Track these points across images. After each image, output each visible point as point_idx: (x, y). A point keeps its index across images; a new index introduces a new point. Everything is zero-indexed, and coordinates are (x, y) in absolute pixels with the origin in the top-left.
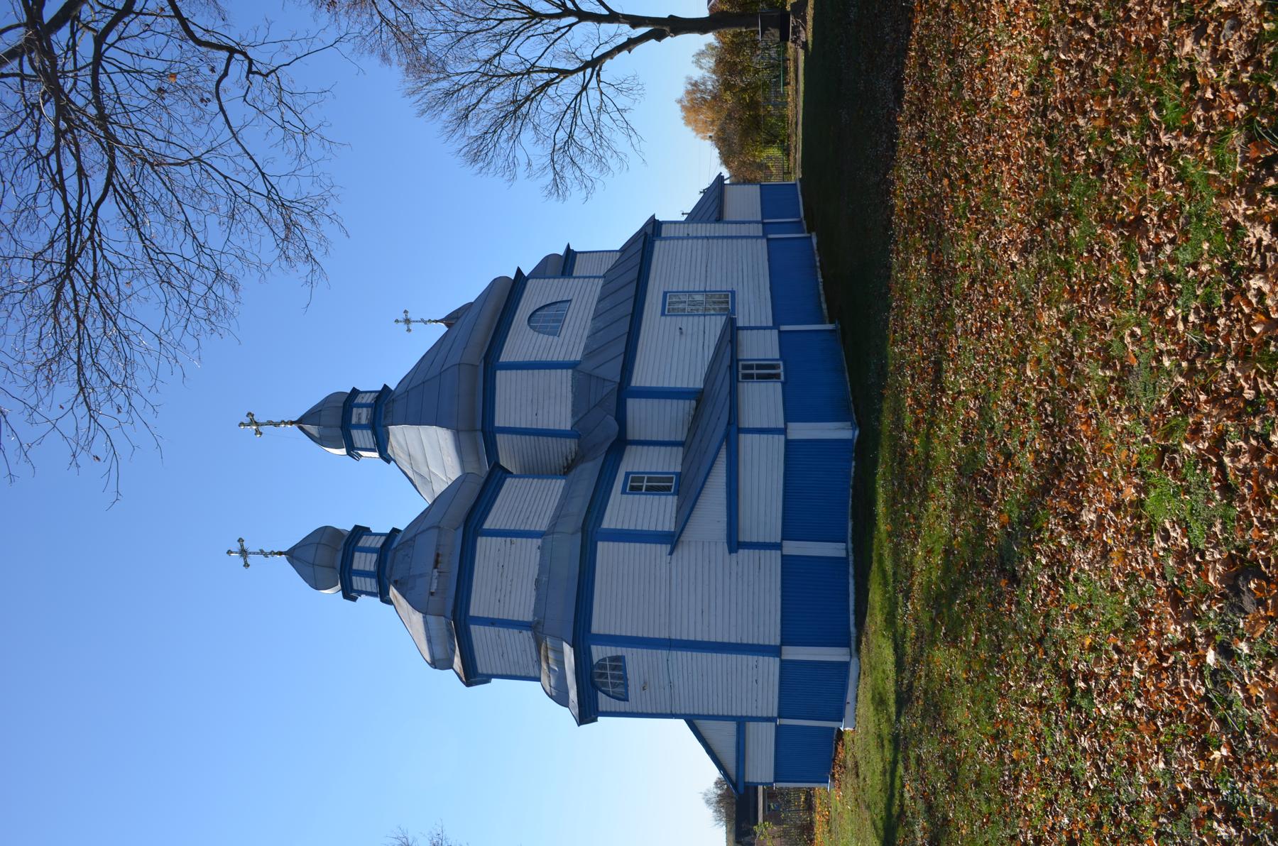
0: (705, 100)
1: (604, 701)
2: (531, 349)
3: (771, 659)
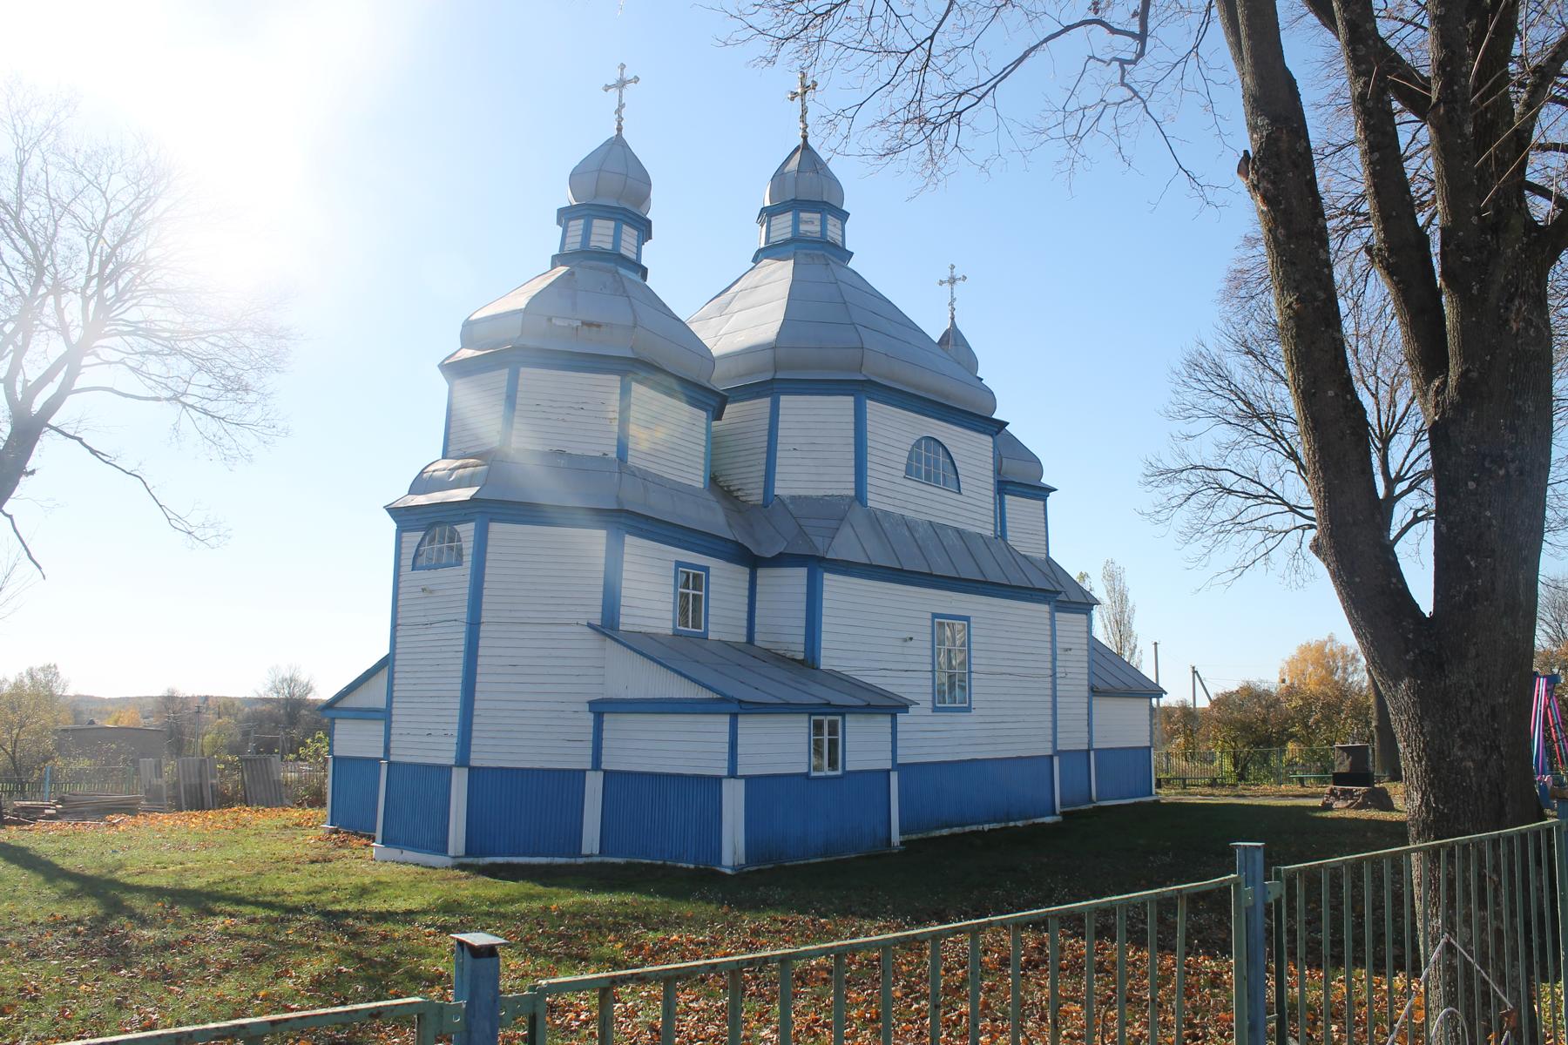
0: (1332, 673)
1: (414, 538)
2: (886, 441)
3: (454, 754)
